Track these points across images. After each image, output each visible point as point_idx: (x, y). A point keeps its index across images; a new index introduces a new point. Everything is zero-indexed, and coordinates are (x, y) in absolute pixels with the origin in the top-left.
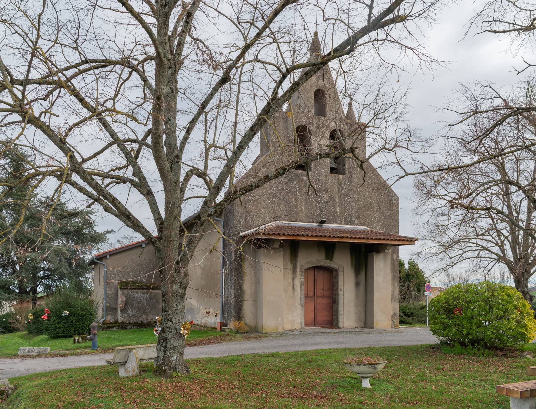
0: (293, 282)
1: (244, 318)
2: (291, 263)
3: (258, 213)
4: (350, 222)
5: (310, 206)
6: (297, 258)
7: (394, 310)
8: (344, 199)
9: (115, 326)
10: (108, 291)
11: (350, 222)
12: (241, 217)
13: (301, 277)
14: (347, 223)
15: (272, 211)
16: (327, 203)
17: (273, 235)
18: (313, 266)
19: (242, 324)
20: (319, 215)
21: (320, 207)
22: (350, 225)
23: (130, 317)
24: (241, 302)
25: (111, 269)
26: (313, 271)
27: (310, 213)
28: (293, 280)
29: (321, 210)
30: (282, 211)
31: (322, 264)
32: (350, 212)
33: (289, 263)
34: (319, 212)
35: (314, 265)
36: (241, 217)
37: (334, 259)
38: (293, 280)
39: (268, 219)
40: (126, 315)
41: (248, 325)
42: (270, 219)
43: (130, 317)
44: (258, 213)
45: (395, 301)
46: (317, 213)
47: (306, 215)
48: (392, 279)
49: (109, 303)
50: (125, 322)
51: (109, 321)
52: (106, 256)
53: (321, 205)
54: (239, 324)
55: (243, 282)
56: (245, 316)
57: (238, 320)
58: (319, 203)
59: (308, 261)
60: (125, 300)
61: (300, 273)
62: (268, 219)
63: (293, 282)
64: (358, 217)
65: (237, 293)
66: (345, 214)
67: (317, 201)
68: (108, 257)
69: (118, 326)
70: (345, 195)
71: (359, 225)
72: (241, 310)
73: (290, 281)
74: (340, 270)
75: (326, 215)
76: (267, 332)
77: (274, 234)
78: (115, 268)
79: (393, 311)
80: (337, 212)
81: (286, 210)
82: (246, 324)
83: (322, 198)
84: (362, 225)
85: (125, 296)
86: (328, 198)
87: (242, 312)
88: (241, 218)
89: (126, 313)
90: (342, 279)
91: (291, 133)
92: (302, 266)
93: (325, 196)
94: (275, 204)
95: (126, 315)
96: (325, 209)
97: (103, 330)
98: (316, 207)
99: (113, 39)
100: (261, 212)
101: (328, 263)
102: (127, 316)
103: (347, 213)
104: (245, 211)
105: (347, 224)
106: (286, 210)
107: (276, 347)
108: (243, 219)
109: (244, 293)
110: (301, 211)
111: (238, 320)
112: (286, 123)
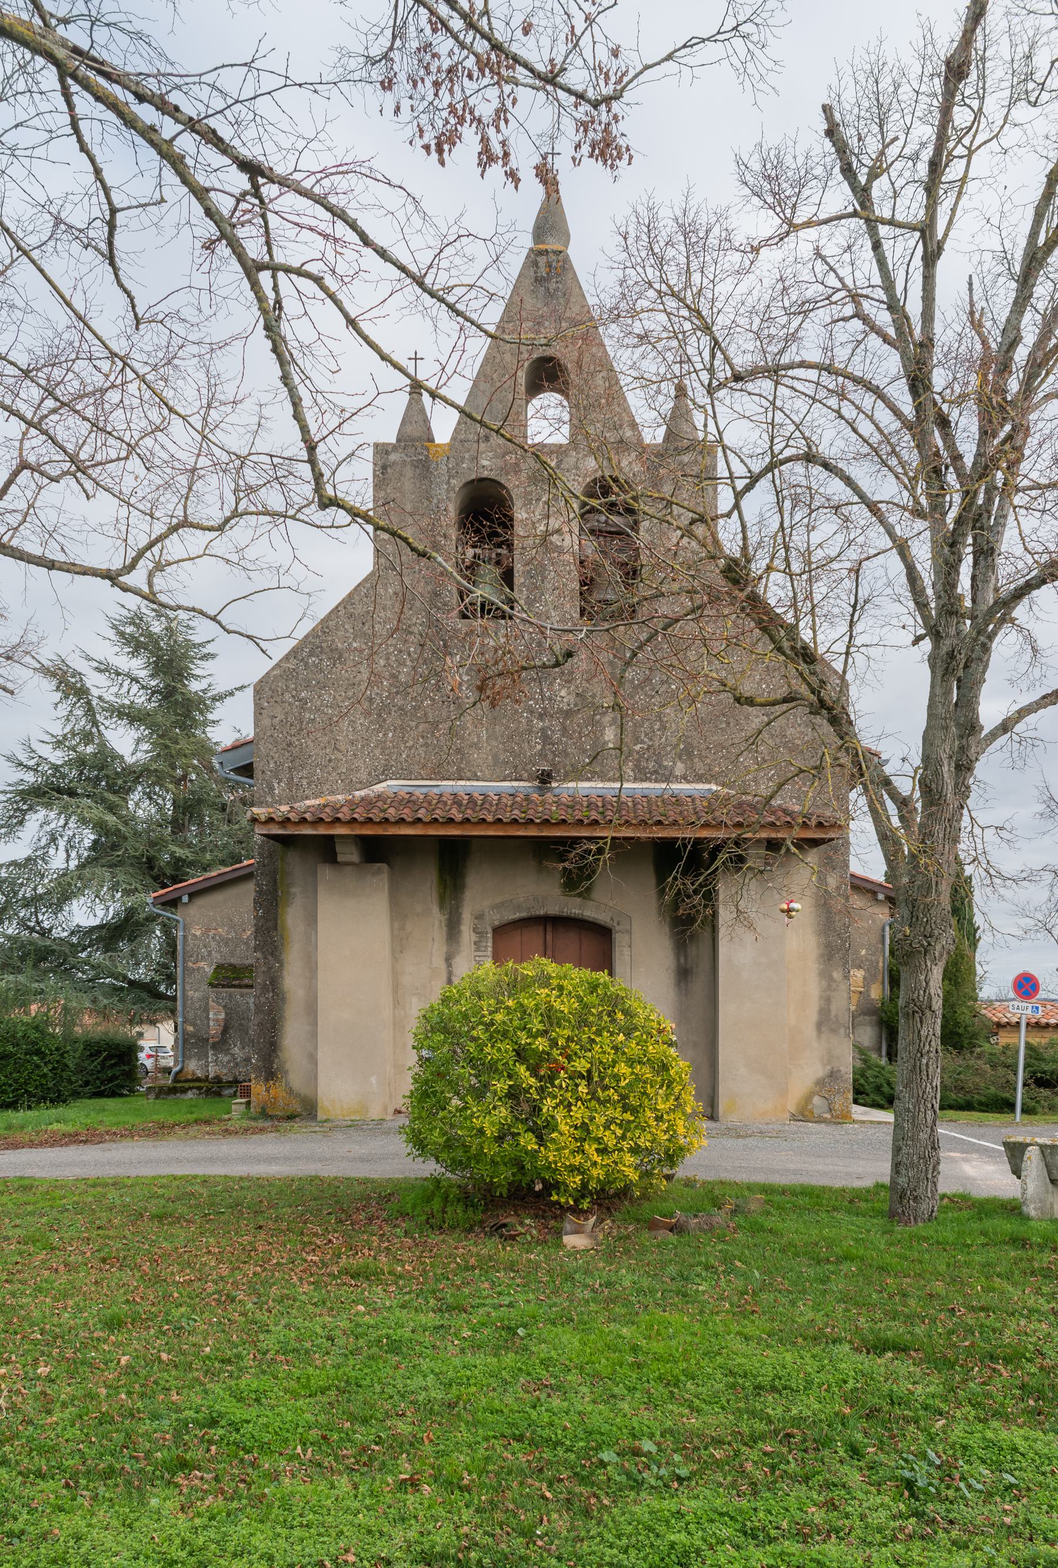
0: (449, 966)
1: (286, 1072)
2: (442, 906)
3: (330, 761)
4: (656, 772)
5: (507, 728)
6: (463, 893)
7: (829, 1062)
8: (632, 697)
9: (190, 1088)
10: (191, 993)
11: (656, 772)
12: (276, 774)
13: (478, 949)
14: (641, 775)
15: (377, 752)
16: (568, 714)
17: (526, 823)
18: (518, 916)
19: (278, 1091)
20: (542, 755)
21: (543, 730)
22: (656, 781)
23: (237, 1064)
24: (274, 1027)
25: (198, 933)
26: (541, 933)
27: (506, 751)
28: (449, 960)
29: (546, 739)
30: (411, 748)
31: (552, 910)
32: (656, 739)
33: (435, 909)
34: (539, 747)
35: (524, 914)
36: (276, 774)
37: (596, 894)
38: (449, 960)
39: (363, 775)
40: (226, 1059)
41: (298, 1095)
42: (370, 774)
43: (237, 1064)
44: (330, 761)
45: (834, 1031)
46: (531, 748)
47: (495, 757)
48: (822, 956)
49: (194, 1025)
50: (225, 1078)
51: (194, 1074)
52: (180, 898)
53: (547, 723)
54: (267, 1090)
55: (282, 965)
56: (288, 1066)
57: (267, 1080)
58: (541, 717)
59: (498, 900)
60: (222, 1016)
61: (474, 937)
62: (363, 775)
63: (449, 966)
64: (687, 754)
65: (263, 1000)
66: (637, 747)
67: (532, 712)
68: (185, 899)
69: (199, 1088)
70: (635, 688)
71: (688, 782)
72: (274, 1051)
73: (439, 963)
74: (618, 928)
75: (567, 755)
76: (331, 1117)
77: (468, 820)
78: (208, 930)
79: (824, 1065)
80: (606, 743)
81: (426, 745)
82: (290, 1091)
83: (550, 699)
84: (700, 778)
85: (225, 1007)
86: (572, 699)
87: (277, 1056)
88: (276, 776)
89: (227, 1052)
90: (628, 958)
91: (442, 506)
92: (479, 917)
93: (563, 693)
94: (389, 729)
95: (226, 1059)
96: (563, 735)
97: (157, 1097)
98: (530, 732)
99: (830, 291)
100: (340, 756)
101: (574, 907)
102: (229, 1062)
103: (642, 742)
104: (287, 754)
105: (642, 780)
106: (426, 745)
107: (362, 1160)
108: (280, 781)
109: (284, 999)
110: (476, 746)
111: (267, 1080)
112: (425, 478)
